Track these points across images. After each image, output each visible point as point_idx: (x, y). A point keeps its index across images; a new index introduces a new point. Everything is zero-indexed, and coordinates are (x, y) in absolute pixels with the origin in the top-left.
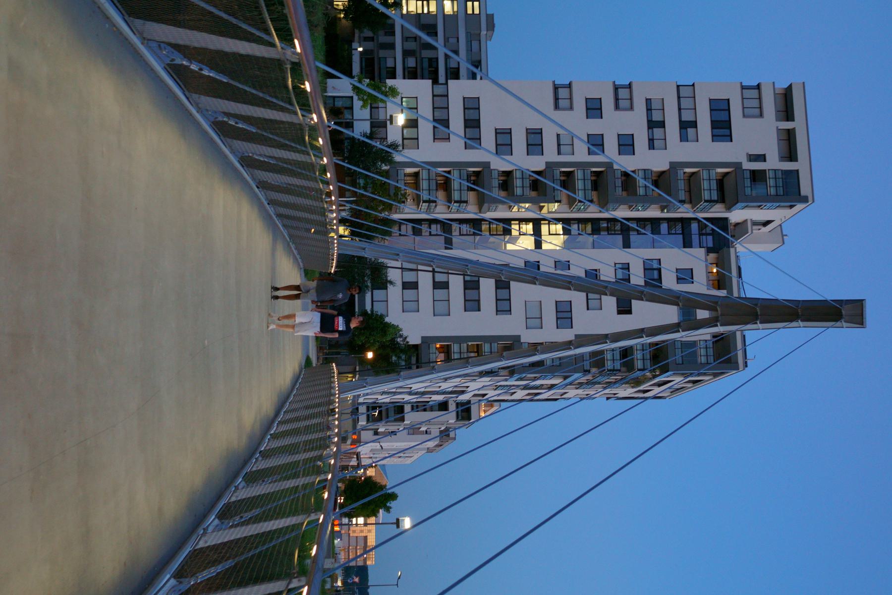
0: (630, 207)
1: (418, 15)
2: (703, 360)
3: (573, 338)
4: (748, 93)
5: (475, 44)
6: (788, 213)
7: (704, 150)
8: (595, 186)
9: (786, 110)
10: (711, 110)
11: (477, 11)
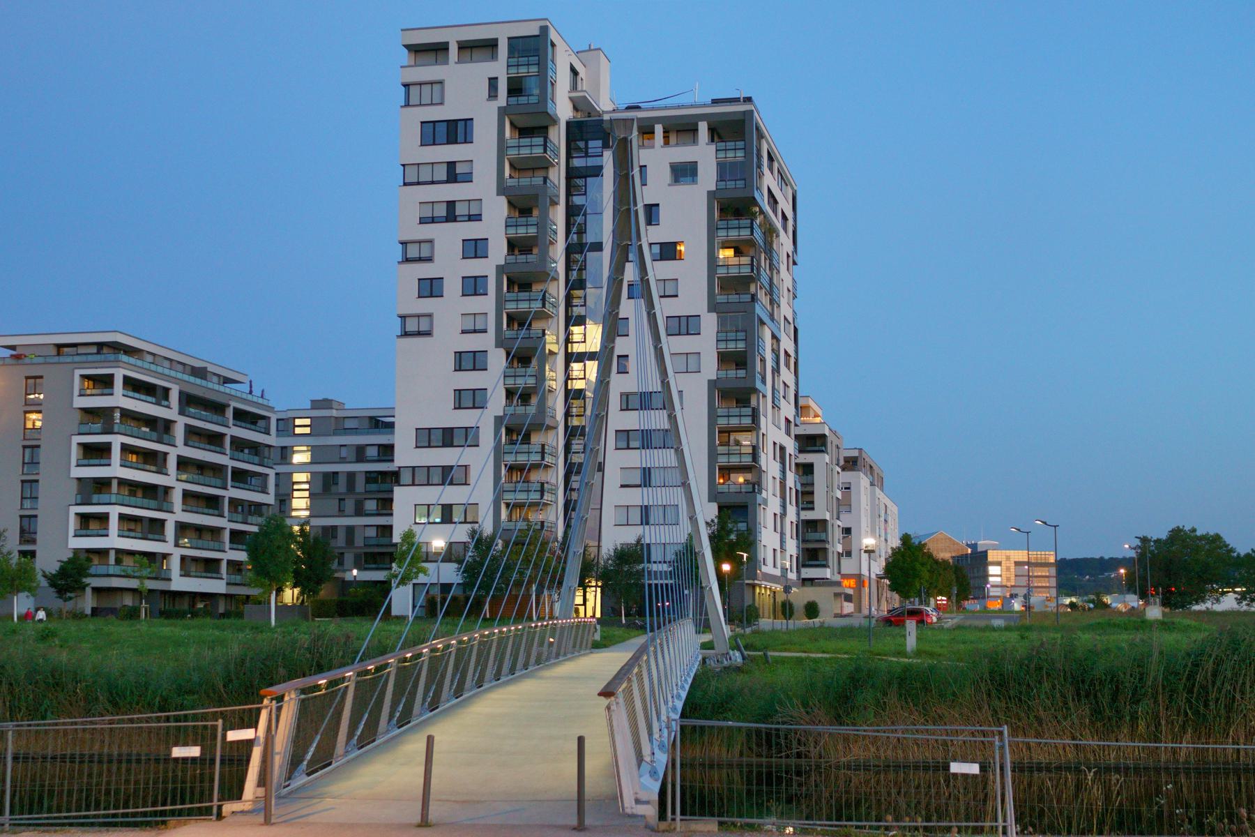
0: (551, 243)
1: (312, 496)
2: (740, 154)
3: (714, 315)
4: (414, 99)
5: (349, 424)
6: (561, 47)
7: (482, 154)
8: (525, 286)
9: (437, 50)
10: (434, 144)
11: (308, 422)
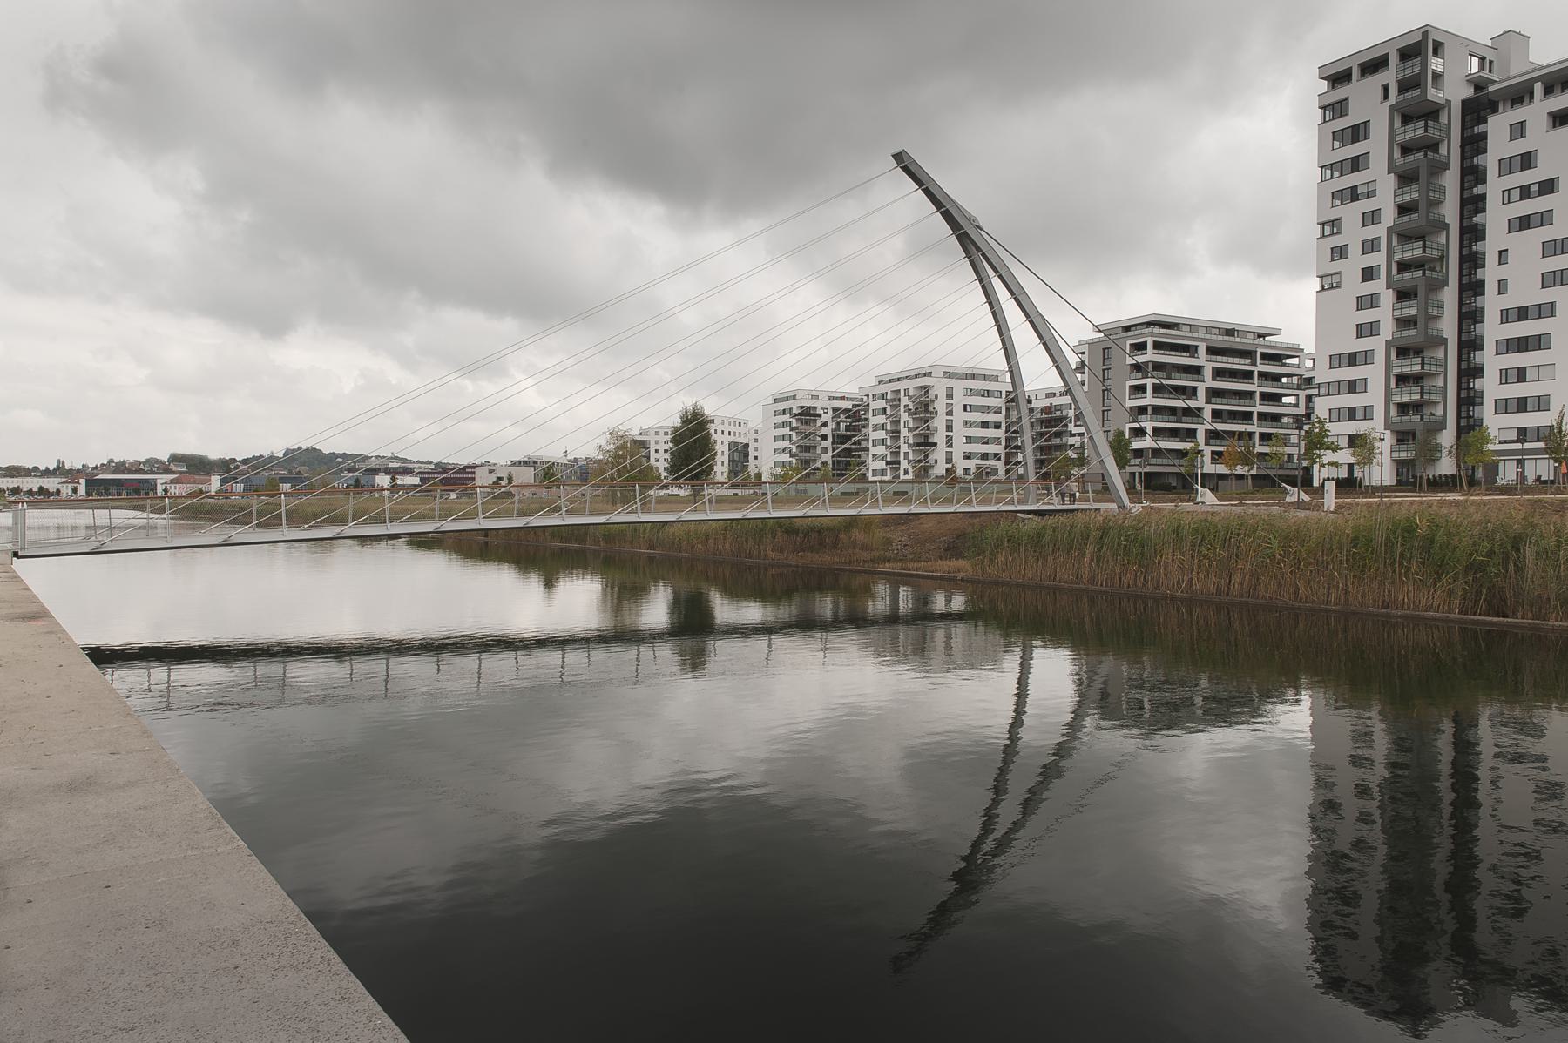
7: (1377, 146)
